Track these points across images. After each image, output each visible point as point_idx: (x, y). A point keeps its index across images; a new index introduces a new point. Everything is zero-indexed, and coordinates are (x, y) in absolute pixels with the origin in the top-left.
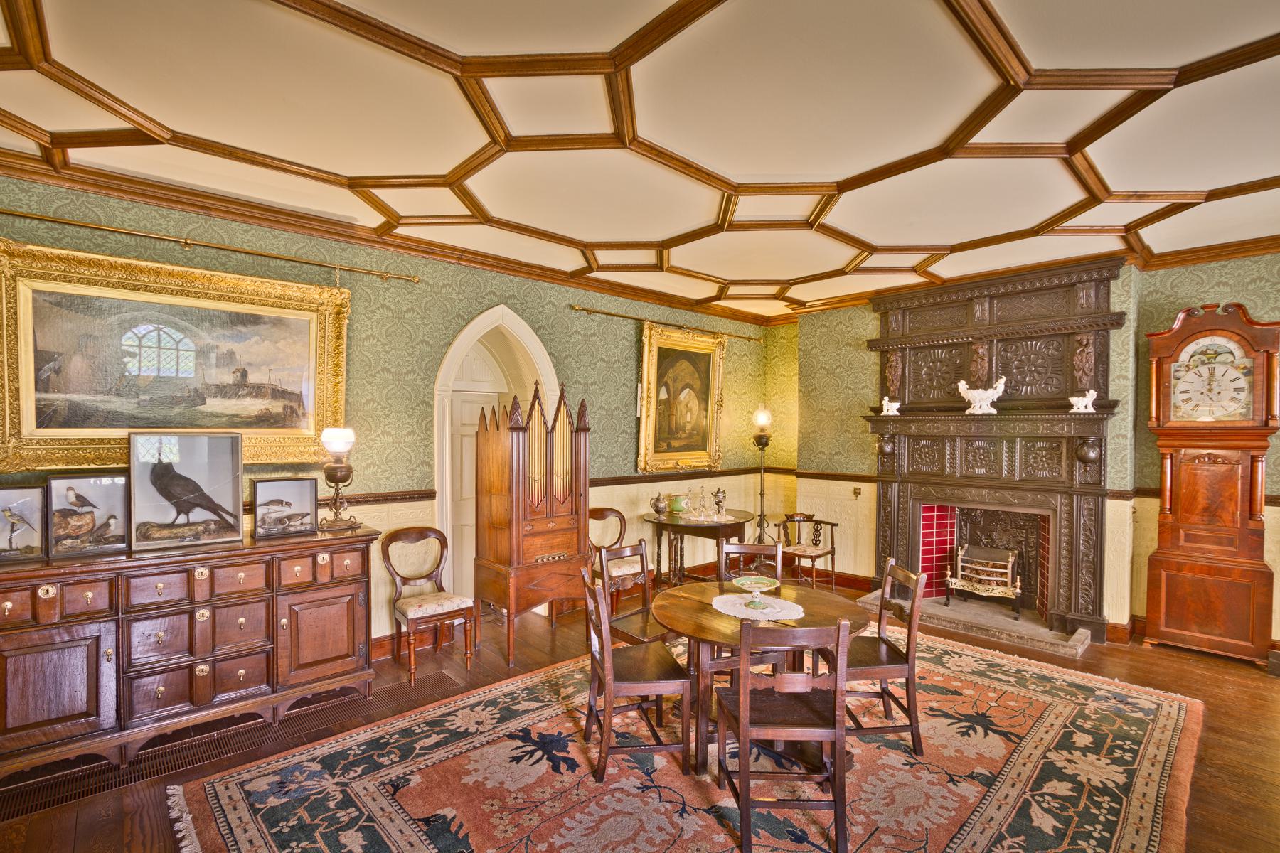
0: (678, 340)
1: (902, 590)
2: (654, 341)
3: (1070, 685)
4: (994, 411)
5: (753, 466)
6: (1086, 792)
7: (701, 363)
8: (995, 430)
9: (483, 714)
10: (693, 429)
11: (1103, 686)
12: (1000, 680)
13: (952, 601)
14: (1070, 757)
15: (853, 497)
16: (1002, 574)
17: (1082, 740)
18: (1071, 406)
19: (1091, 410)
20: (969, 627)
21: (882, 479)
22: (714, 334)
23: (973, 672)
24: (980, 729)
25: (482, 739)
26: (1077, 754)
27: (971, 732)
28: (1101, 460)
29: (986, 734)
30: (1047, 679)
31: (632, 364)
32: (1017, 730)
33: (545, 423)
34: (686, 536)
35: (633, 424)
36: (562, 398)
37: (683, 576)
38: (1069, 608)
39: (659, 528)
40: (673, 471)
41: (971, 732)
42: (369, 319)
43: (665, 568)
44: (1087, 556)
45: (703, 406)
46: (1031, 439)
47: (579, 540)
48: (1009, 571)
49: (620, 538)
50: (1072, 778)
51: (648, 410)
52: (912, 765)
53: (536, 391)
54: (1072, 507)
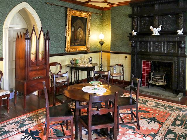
0: (77, 14)
1: (136, 84)
2: (71, 13)
3: (177, 108)
4: (159, 34)
5: (99, 50)
6: (177, 137)
7: (84, 21)
8: (160, 39)
9: (15, 126)
10: (81, 39)
11: (185, 108)
12: (160, 108)
13: (150, 87)
14: (175, 127)
15: (125, 58)
16: (162, 79)
17: (178, 122)
18: (177, 33)
19: (182, 34)
20: (153, 94)
21: (132, 53)
22: (88, 12)
23: (153, 106)
24: (153, 121)
25: (13, 133)
26: (176, 126)
27: (151, 122)
28: (185, 47)
29: (155, 123)
30: (171, 107)
31: (64, 20)
32: (162, 121)
33: (36, 37)
34: (79, 71)
35: (64, 38)
36: (41, 30)
37: (78, 82)
38: (177, 87)
39: (72, 68)
40: (76, 52)
41: (151, 122)
42: (7, 8)
43: (73, 81)
44: (182, 73)
45: (85, 33)
46: (169, 42)
47: (46, 72)
48: (163, 78)
49: (60, 71)
50: (175, 133)
51: (68, 34)
52: (134, 133)
53: (34, 27)
54: (178, 60)
